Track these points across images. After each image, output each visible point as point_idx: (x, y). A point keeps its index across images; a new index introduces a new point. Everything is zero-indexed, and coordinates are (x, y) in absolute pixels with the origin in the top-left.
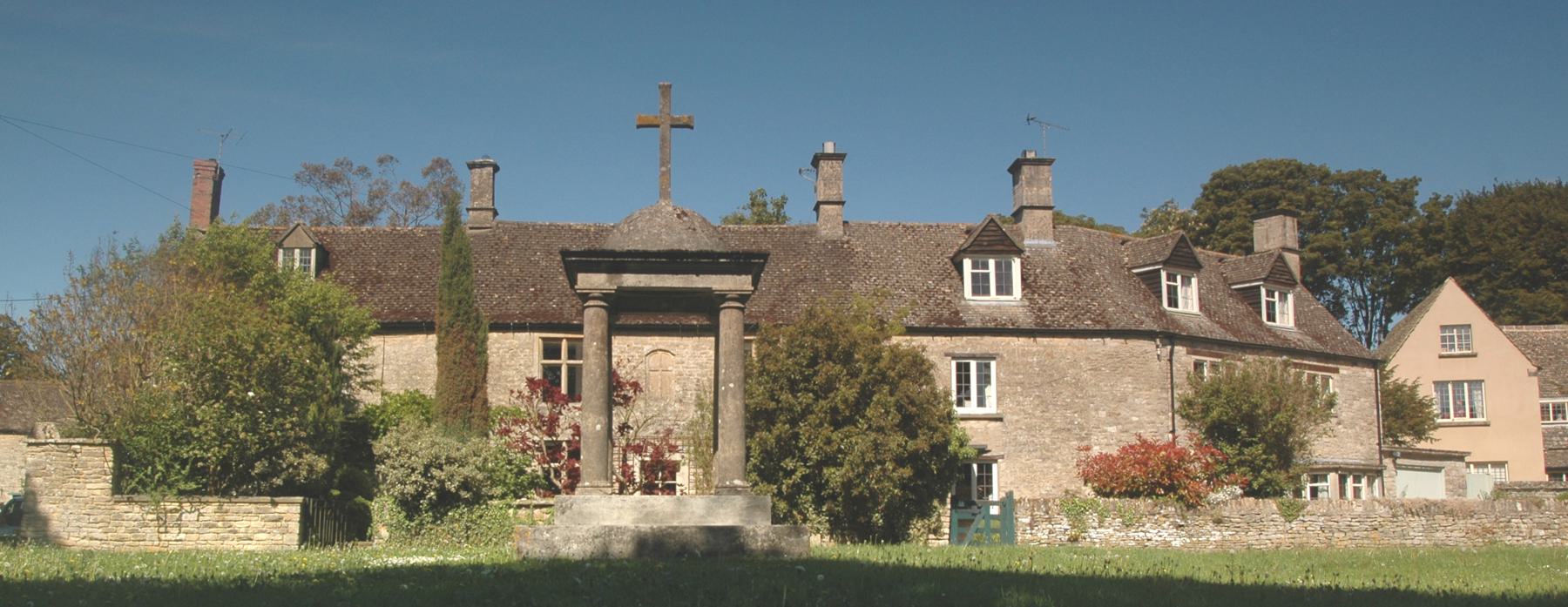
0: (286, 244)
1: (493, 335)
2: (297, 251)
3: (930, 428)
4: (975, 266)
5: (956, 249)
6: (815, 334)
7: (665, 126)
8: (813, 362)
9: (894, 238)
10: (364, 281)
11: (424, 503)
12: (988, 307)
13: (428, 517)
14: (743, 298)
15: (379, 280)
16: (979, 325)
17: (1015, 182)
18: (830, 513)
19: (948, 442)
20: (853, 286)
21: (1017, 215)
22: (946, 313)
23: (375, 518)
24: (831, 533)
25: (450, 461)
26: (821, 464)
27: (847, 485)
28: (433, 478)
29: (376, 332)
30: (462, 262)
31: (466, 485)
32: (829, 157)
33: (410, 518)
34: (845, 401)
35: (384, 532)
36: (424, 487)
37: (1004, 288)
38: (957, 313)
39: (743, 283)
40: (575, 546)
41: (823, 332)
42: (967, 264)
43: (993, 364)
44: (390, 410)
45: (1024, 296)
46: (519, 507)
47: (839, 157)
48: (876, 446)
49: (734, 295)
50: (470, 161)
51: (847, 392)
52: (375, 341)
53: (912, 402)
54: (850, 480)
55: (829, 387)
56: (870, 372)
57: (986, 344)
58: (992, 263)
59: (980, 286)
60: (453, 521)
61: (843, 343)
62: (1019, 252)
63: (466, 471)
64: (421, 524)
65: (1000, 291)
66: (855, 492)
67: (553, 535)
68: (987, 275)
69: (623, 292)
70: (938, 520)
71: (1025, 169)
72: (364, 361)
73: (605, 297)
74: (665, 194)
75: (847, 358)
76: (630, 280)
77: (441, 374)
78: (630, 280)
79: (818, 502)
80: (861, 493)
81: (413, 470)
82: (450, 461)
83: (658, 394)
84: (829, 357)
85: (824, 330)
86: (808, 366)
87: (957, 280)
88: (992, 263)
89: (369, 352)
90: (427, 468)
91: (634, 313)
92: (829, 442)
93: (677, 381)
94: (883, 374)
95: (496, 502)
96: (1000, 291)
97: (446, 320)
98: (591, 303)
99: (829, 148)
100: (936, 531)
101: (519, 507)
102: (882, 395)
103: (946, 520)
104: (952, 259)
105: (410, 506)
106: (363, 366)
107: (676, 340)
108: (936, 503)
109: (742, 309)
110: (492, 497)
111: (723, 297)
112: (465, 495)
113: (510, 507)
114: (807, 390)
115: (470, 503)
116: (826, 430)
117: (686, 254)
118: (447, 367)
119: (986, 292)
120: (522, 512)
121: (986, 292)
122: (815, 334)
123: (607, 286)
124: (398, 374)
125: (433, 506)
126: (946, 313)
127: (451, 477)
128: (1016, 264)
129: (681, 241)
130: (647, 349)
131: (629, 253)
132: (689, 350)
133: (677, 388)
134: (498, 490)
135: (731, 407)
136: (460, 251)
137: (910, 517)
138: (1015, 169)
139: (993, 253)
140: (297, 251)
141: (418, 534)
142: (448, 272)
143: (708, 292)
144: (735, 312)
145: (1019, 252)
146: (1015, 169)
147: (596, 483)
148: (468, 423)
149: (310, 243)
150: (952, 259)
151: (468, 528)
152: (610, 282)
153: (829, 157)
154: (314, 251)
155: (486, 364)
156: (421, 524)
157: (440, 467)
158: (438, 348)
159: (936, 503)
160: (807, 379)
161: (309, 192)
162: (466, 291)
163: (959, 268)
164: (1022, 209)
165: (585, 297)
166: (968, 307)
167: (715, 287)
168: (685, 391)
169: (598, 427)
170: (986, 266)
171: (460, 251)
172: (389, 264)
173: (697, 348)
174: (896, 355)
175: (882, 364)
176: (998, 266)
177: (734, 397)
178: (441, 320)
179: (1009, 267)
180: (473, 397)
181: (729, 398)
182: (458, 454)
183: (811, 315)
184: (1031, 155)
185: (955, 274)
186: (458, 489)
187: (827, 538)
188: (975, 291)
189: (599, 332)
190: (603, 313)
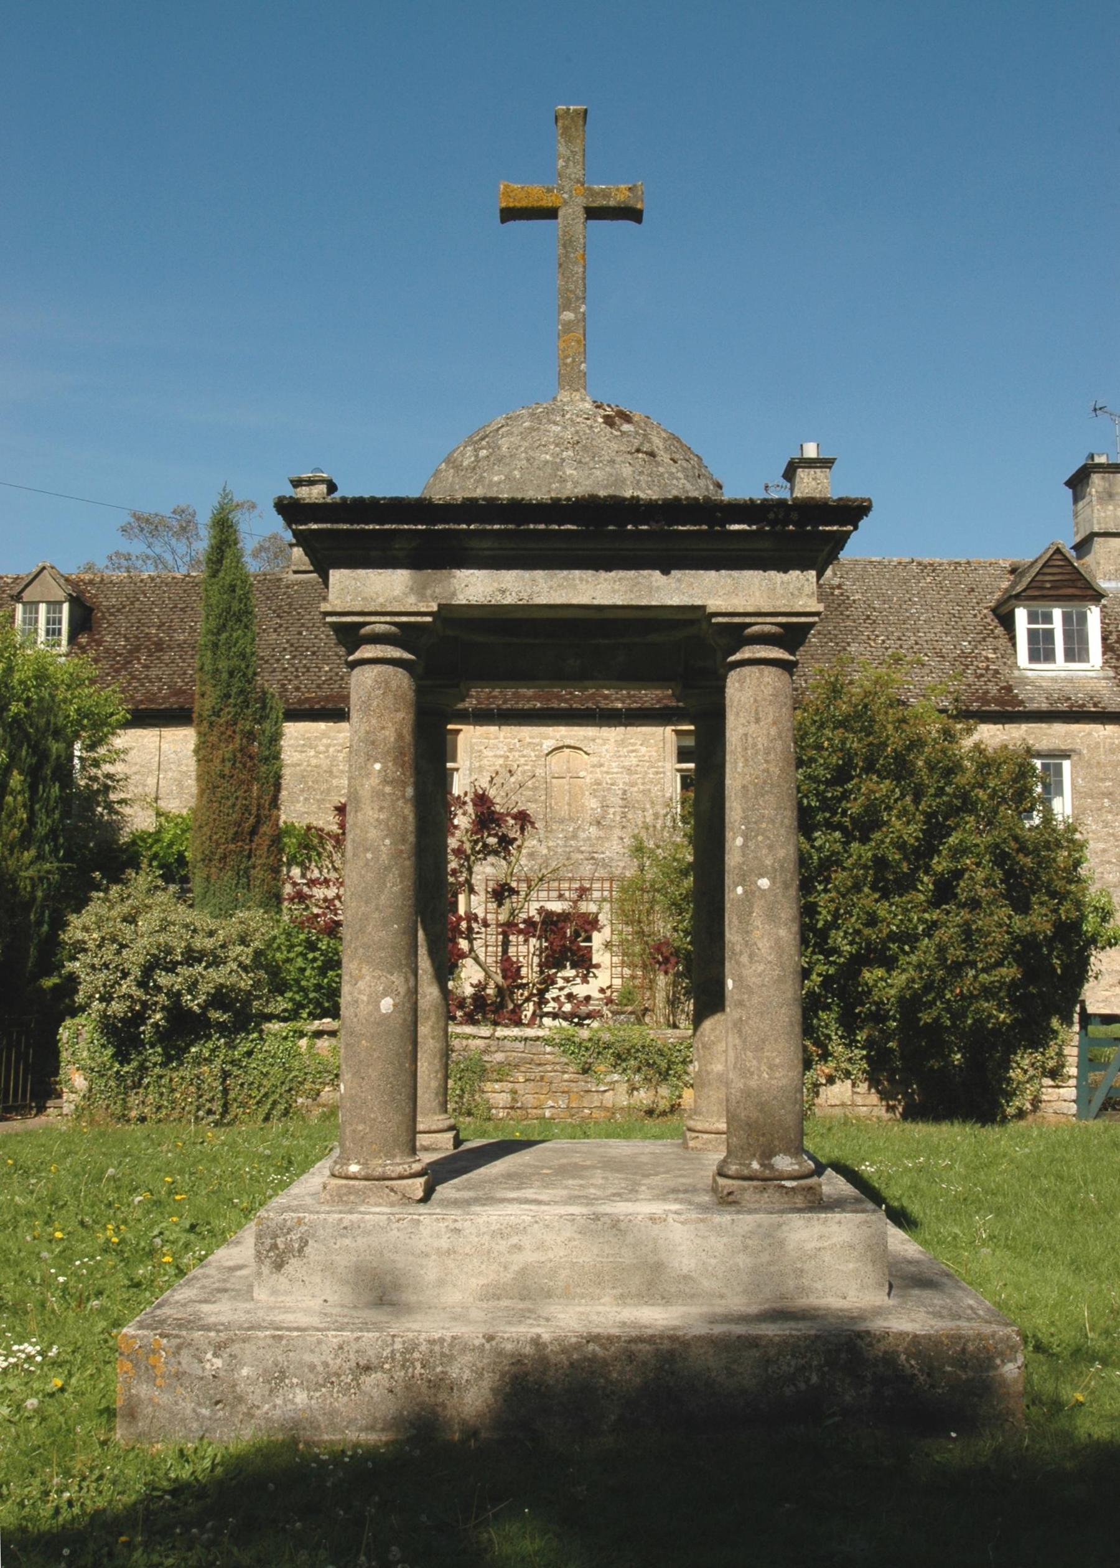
0: (26, 596)
1: (293, 731)
2: (43, 608)
3: (1053, 894)
4: (1033, 618)
5: (997, 595)
6: (843, 724)
7: (572, 214)
8: (842, 775)
9: (906, 581)
10: (137, 649)
11: (146, 1031)
12: (1054, 680)
13: (154, 1054)
14: (792, 634)
15: (159, 646)
16: (1044, 706)
17: (1076, 500)
18: (869, 1044)
19: (1083, 918)
20: (853, 648)
21: (1083, 547)
22: (993, 690)
23: (65, 1055)
24: (873, 1081)
25: (192, 957)
26: (858, 961)
27: (910, 1004)
28: (158, 988)
29: (128, 725)
30: (236, 606)
31: (220, 998)
32: (810, 463)
33: (122, 1057)
34: (901, 846)
35: (79, 1081)
36: (144, 1004)
37: (1076, 650)
38: (1009, 689)
39: (787, 591)
40: (301, 1398)
41: (860, 719)
42: (1021, 615)
43: (1066, 765)
44: (167, 837)
45: (1105, 662)
46: (318, 1034)
47: (824, 463)
48: (967, 933)
49: (765, 627)
50: (295, 476)
51: (903, 828)
52: (123, 739)
53: (1022, 849)
54: (916, 997)
55: (866, 826)
56: (940, 792)
57: (1054, 735)
58: (1057, 614)
59: (1041, 649)
60: (198, 1061)
61: (895, 742)
62: (1097, 596)
63: (218, 976)
64: (143, 1069)
65: (1070, 656)
66: (926, 1018)
67: (234, 1362)
68: (1051, 631)
69: (451, 617)
70: (1060, 1054)
71: (1096, 479)
72: (107, 768)
73: (407, 634)
74: (572, 379)
75: (900, 769)
76: (476, 587)
77: (202, 792)
78: (476, 587)
79: (849, 1024)
80: (937, 1020)
81: (125, 975)
82: (192, 957)
83: (564, 812)
84: (870, 768)
85: (859, 716)
86: (829, 783)
87: (1003, 642)
88: (1057, 614)
89: (118, 755)
90: (148, 970)
91: (464, 669)
92: (872, 920)
93: (593, 793)
94: (965, 796)
95: (274, 1026)
96: (1071, 655)
97: (208, 703)
98: (367, 652)
99: (811, 451)
100: (1055, 1074)
101: (318, 1034)
102: (967, 832)
103: (1072, 1052)
104: (994, 610)
105: (123, 1036)
106: (109, 776)
107: (590, 731)
108: (1055, 1023)
109: (788, 667)
110: (269, 1018)
111: (735, 633)
112: (215, 1015)
113: (302, 1035)
114: (831, 826)
115: (230, 1031)
116: (867, 899)
117: (634, 509)
118: (211, 783)
119: (1050, 657)
120: (323, 1043)
121: (1050, 657)
122: (843, 724)
123: (411, 603)
124: (180, 785)
125: (163, 1036)
126: (993, 690)
127: (192, 987)
128: (1094, 616)
129: (620, 481)
130: (548, 745)
131: (471, 509)
132: (611, 746)
133: (594, 803)
134: (281, 1004)
135: (764, 946)
136: (233, 588)
137: (1011, 1049)
138: (1078, 482)
139: (1058, 599)
140: (43, 608)
141: (137, 1085)
142: (213, 624)
143: (693, 618)
144: (771, 675)
145: (1097, 596)
146: (1078, 482)
147: (379, 1166)
148: (244, 876)
149: (61, 595)
150: (994, 610)
151: (226, 1075)
152: (420, 590)
153: (810, 463)
154: (66, 607)
155: (278, 777)
156: (143, 1069)
157: (171, 968)
158: (196, 752)
159: (1055, 1023)
160: (827, 805)
161: (137, 547)
162: (243, 656)
163: (1008, 622)
164: (1093, 535)
165: (350, 635)
166: (1024, 681)
167: (715, 604)
168: (605, 807)
169: (387, 1004)
170: (1048, 618)
171: (233, 588)
172: (176, 624)
173: (622, 743)
174: (987, 764)
175: (960, 780)
176: (1067, 618)
177: (771, 916)
178: (204, 705)
179: (1083, 619)
180: (253, 832)
181: (757, 919)
182: (209, 943)
183: (835, 691)
184: (1101, 460)
185: (1000, 631)
186: (204, 1008)
187: (863, 1087)
188: (1034, 657)
189: (389, 734)
190: (401, 679)
